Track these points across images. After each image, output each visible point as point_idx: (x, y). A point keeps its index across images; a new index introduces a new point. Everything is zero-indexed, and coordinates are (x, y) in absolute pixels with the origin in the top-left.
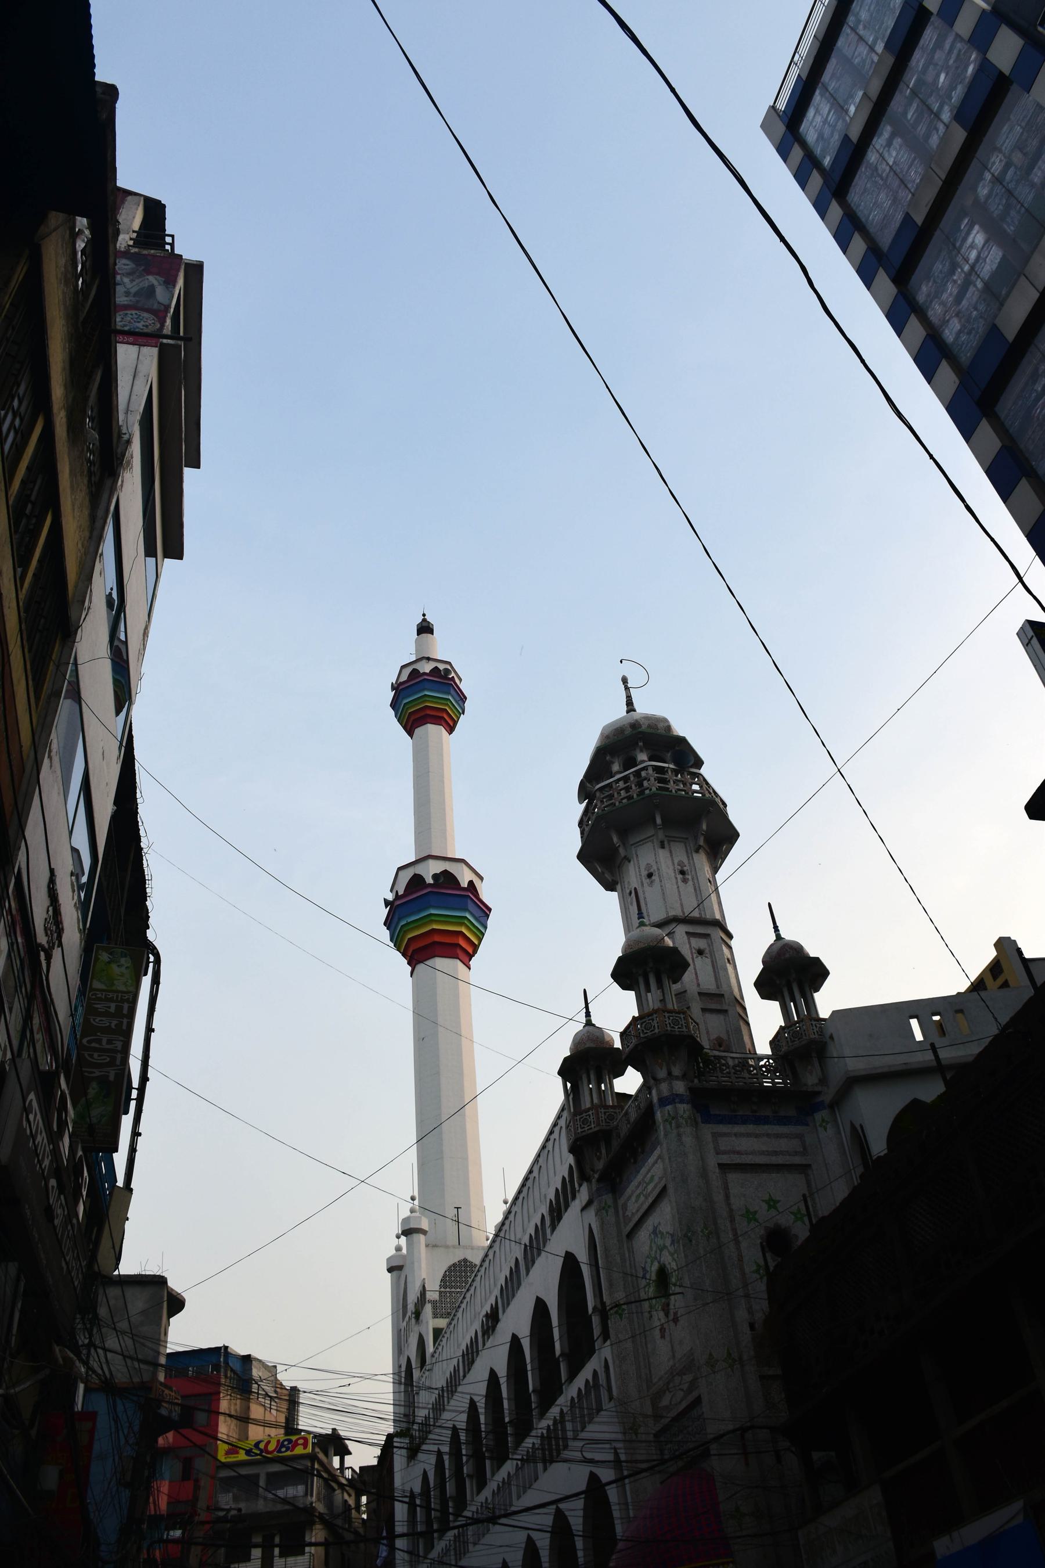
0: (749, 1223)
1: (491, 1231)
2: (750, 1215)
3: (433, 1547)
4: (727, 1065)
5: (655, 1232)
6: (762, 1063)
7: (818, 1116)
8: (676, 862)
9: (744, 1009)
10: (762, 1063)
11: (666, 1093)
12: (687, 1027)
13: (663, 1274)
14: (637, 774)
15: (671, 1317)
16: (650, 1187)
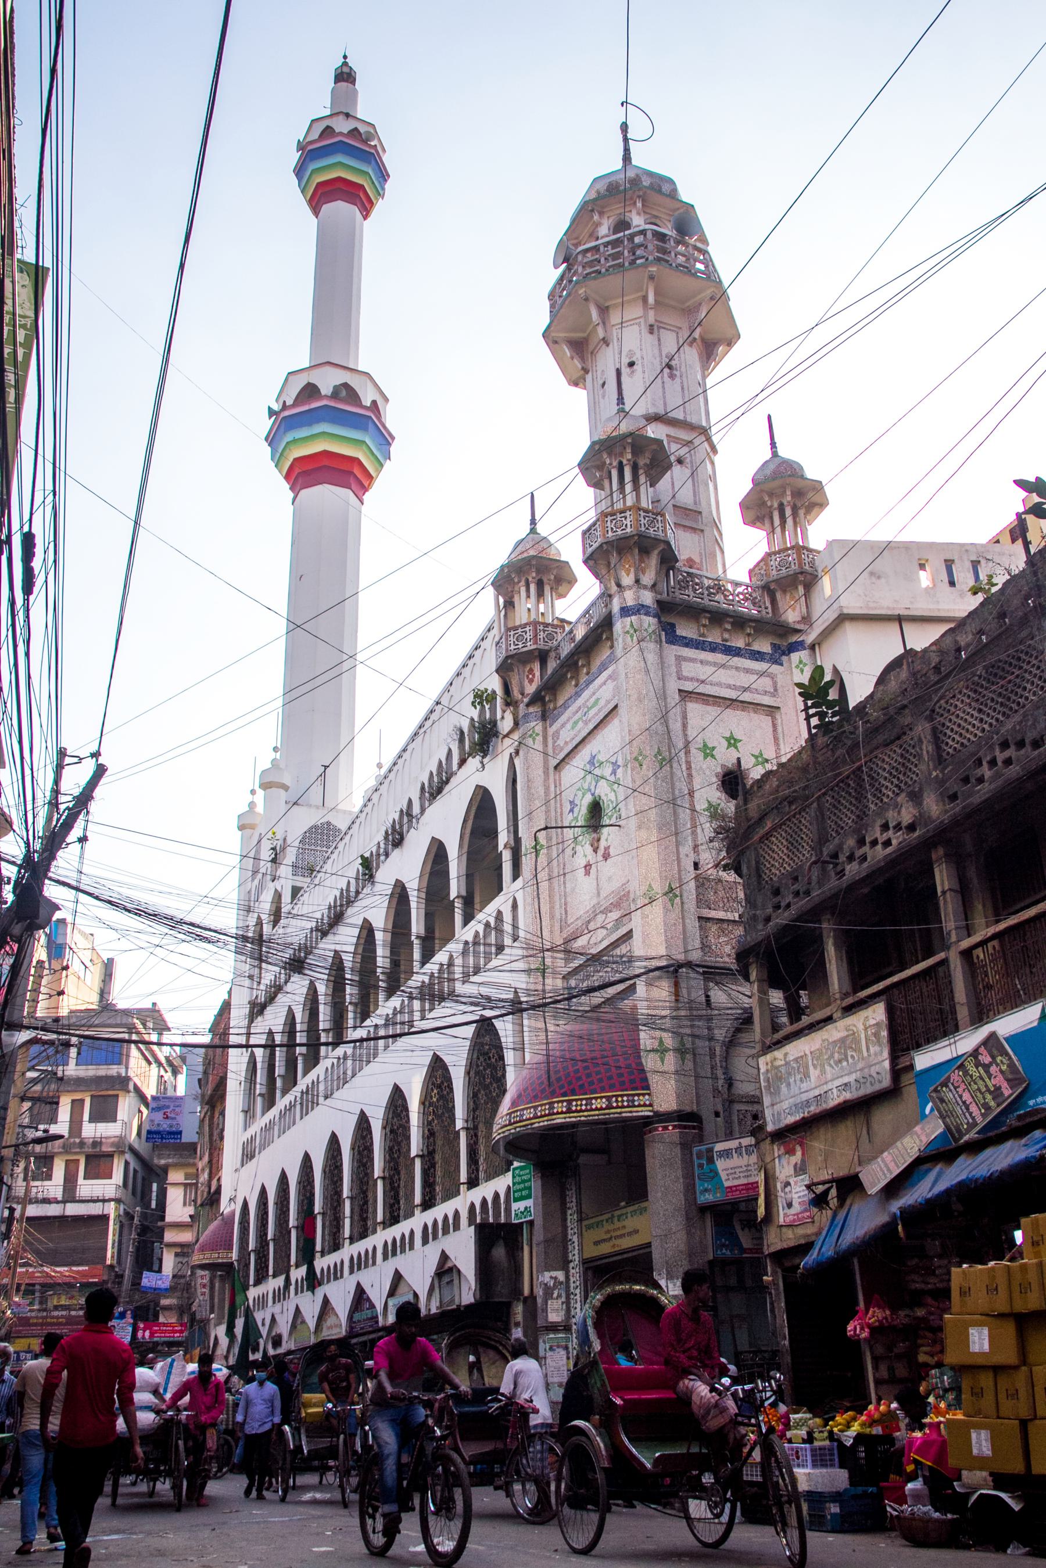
0: (705, 758)
1: (358, 802)
2: (708, 752)
3: (295, 1084)
4: (701, 585)
5: (591, 762)
6: (740, 590)
7: (795, 657)
8: (664, 355)
9: (721, 535)
10: (740, 590)
11: (630, 603)
12: (664, 531)
13: (596, 809)
14: (631, 238)
15: (601, 851)
16: (592, 712)
